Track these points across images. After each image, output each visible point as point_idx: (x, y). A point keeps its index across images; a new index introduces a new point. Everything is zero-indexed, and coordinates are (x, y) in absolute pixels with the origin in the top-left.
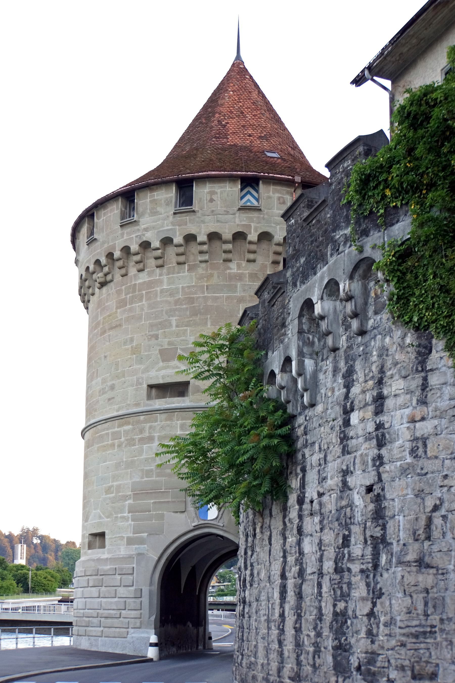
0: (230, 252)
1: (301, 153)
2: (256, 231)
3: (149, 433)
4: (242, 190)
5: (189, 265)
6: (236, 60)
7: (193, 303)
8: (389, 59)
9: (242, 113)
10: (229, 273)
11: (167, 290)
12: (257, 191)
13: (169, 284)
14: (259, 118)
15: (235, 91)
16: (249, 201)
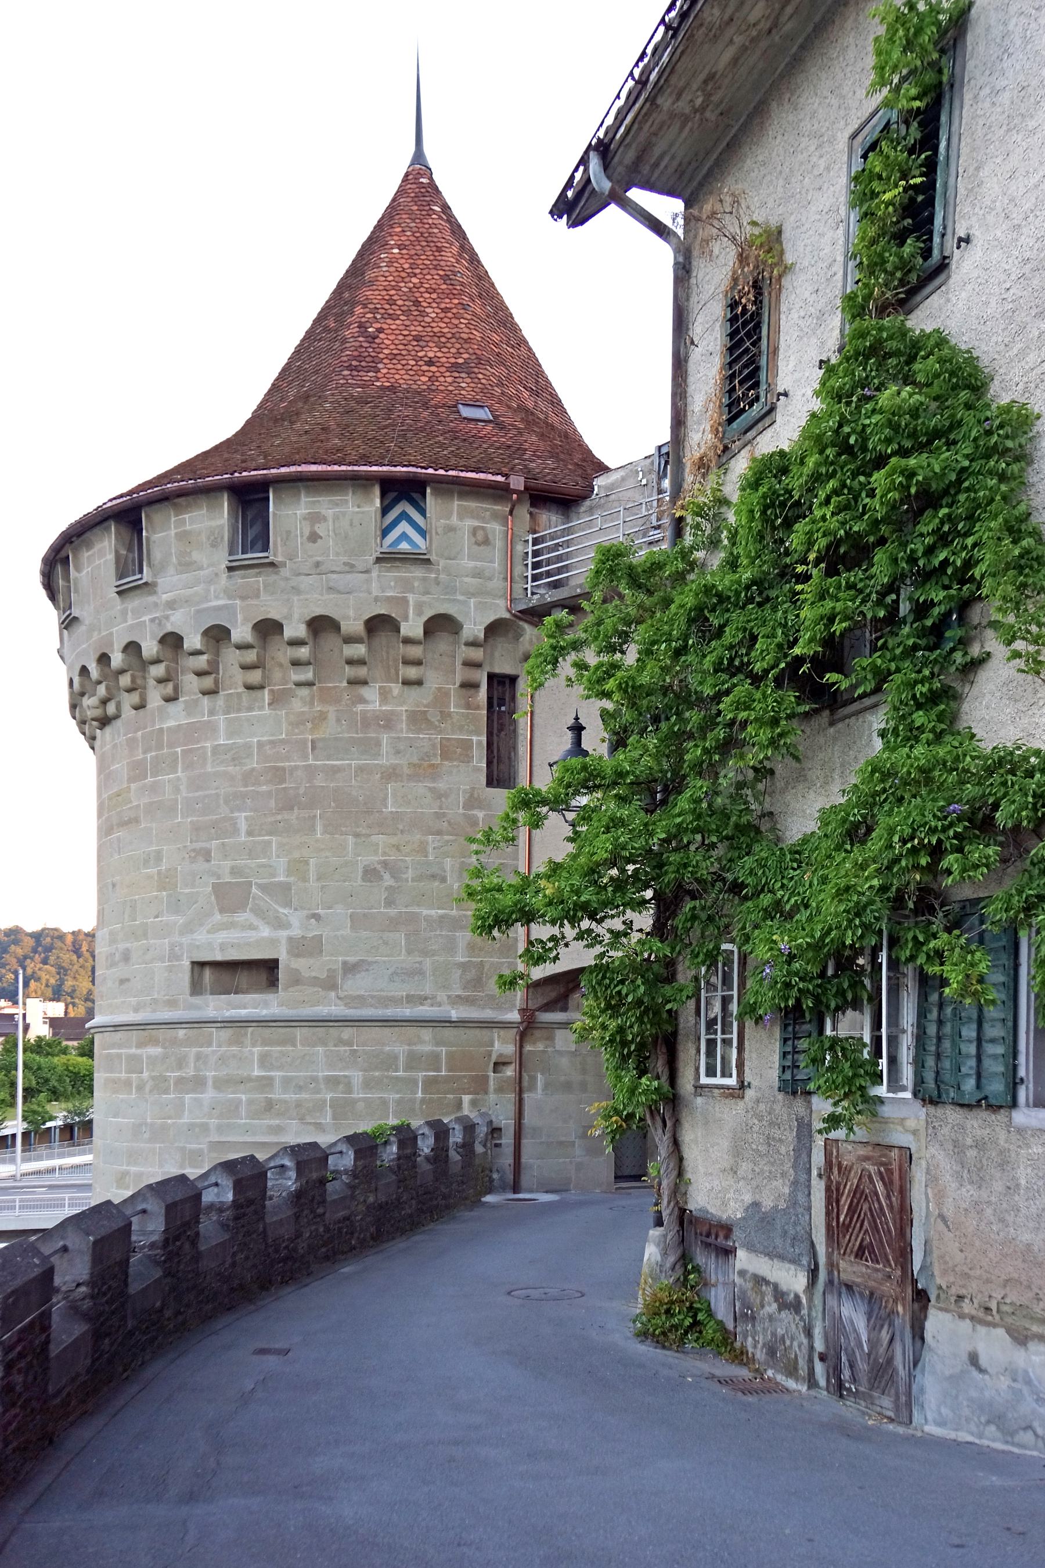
0: (361, 662)
1: (555, 402)
2: (419, 614)
3: (196, 1069)
4: (385, 511)
5: (272, 691)
6: (412, 164)
7: (283, 781)
8: (665, 102)
9: (416, 303)
10: (364, 713)
11: (228, 749)
12: (423, 512)
13: (230, 735)
14: (456, 316)
15: (405, 247)
16: (404, 536)
